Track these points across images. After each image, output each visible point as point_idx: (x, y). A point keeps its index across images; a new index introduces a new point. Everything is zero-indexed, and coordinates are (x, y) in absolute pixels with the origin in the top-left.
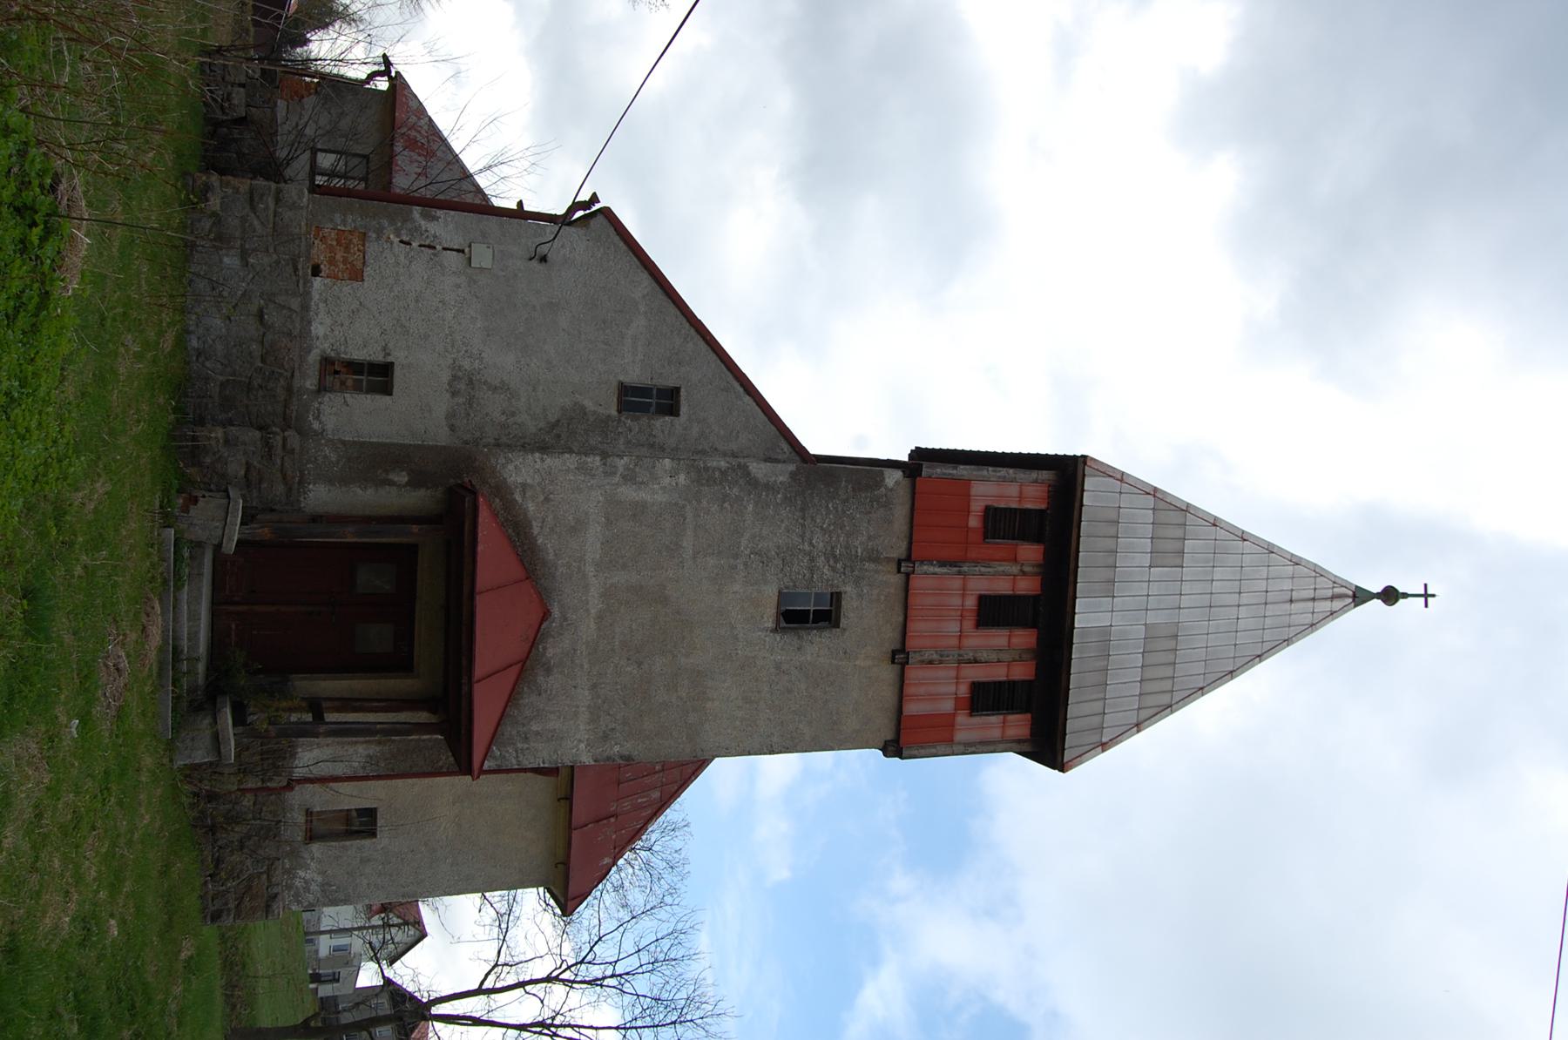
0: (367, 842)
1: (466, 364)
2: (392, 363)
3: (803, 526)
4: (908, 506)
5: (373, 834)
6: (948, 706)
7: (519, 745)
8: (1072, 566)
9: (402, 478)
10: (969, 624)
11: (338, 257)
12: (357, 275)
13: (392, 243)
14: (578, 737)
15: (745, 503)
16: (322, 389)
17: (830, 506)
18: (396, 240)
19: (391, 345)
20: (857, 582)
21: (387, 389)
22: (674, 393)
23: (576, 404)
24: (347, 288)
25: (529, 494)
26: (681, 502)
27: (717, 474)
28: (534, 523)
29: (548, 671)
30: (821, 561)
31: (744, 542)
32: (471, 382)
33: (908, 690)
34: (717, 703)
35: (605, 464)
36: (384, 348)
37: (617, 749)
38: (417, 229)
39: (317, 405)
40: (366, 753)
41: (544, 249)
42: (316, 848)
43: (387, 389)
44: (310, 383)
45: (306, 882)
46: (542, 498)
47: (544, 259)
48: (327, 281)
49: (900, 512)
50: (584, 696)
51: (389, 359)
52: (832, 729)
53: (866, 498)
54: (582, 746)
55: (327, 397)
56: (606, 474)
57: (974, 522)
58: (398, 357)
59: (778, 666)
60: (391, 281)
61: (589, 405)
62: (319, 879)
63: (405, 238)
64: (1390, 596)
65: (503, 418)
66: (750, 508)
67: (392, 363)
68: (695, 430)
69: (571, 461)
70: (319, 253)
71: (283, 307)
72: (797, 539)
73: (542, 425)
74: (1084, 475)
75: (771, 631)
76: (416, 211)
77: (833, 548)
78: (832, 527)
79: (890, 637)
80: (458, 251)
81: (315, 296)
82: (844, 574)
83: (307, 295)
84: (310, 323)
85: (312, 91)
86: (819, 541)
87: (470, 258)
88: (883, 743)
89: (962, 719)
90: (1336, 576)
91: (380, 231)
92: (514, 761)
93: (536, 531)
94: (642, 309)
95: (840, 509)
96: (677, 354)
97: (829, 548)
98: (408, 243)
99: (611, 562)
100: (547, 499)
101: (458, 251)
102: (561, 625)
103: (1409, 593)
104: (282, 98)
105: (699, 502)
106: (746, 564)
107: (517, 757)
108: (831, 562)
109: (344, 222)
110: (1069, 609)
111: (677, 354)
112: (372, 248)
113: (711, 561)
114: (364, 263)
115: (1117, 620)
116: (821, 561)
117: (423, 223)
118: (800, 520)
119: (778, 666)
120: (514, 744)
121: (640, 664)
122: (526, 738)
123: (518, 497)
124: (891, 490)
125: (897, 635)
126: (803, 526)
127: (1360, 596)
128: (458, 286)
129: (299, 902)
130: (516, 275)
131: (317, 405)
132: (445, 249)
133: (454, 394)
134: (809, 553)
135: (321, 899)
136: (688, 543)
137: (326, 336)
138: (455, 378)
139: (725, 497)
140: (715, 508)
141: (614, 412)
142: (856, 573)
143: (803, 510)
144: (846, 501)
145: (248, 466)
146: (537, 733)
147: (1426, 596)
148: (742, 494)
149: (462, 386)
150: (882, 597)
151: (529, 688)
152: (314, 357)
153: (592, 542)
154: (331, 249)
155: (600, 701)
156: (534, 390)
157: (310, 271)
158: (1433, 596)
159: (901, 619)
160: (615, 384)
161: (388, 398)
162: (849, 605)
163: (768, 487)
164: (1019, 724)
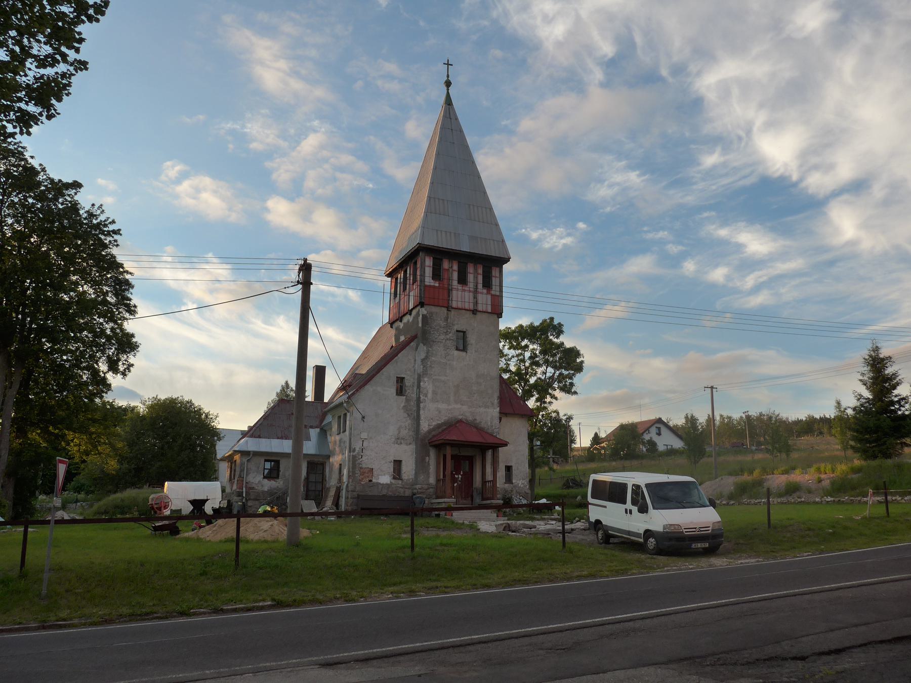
1: (393, 440)
3: (438, 342)
6: (489, 297)
8: (450, 250)
21: (400, 461)
24: (375, 473)
25: (430, 424)
26: (432, 380)
29: (475, 419)
30: (448, 337)
31: (442, 361)
32: (398, 439)
33: (484, 310)
34: (485, 371)
37: (496, 401)
42: (514, 481)
44: (400, 482)
46: (432, 421)
50: (482, 410)
58: (392, 459)
61: (403, 404)
62: (521, 480)
64: (448, 84)
66: (433, 358)
68: (408, 372)
79: (469, 314)
86: (442, 337)
91: (360, 464)
98: (362, 456)
100: (432, 419)
105: (432, 374)
106: (449, 360)
109: (358, 474)
110: (463, 253)
112: (364, 466)
116: (448, 337)
119: (476, 351)
121: (474, 393)
125: (468, 312)
126: (438, 342)
127: (448, 101)
133: (401, 443)
134: (446, 340)
136: (443, 378)
139: (430, 366)
149: (399, 441)
152: (393, 481)
153: (443, 406)
158: (452, 65)
164: (495, 272)
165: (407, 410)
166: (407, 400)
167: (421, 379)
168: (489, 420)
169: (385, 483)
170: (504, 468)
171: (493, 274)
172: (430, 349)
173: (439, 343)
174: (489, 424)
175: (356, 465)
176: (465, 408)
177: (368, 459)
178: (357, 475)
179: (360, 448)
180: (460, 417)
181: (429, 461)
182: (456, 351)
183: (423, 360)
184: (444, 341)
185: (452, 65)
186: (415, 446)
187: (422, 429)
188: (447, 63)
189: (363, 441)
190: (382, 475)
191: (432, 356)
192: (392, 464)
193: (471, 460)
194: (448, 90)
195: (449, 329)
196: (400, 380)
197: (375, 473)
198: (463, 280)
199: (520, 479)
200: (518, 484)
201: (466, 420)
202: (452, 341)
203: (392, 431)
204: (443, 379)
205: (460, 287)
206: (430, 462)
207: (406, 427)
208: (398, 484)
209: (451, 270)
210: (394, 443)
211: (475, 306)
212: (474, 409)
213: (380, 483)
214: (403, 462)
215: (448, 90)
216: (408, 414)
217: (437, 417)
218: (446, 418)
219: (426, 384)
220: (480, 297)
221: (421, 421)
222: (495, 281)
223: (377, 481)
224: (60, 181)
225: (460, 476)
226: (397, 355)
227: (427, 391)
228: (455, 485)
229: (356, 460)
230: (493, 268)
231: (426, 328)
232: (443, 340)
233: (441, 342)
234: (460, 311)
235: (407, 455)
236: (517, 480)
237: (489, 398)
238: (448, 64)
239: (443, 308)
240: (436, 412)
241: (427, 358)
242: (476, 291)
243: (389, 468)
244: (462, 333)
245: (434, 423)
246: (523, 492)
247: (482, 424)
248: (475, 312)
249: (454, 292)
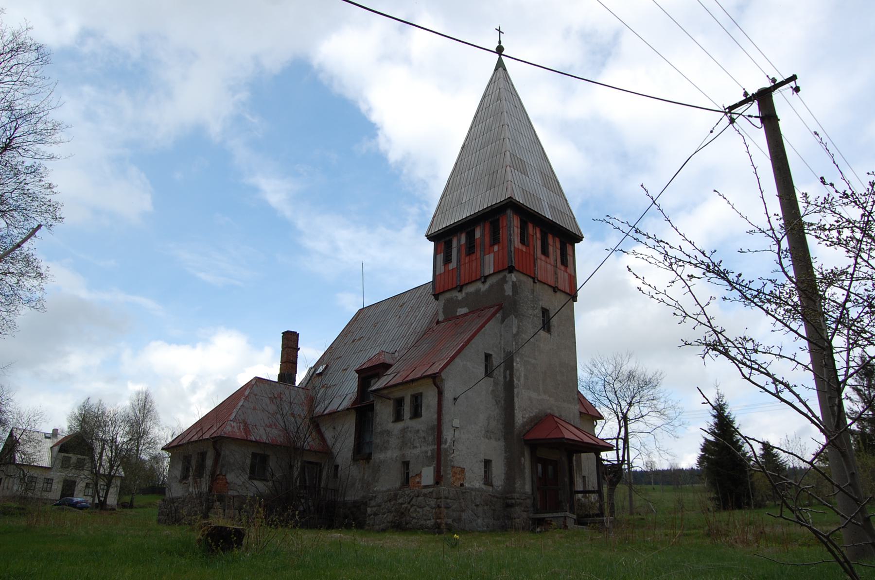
5: (464, 468)
6: (566, 275)
9: (523, 459)
12: (463, 470)
16: (492, 486)
18: (453, 455)
32: (488, 431)
51: (483, 461)
55: (494, 483)
61: (491, 388)
67: (485, 459)
70: (458, 484)
76: (443, 446)
79: (550, 291)
81: (469, 486)
83: (469, 488)
84: (476, 488)
85: (224, 478)
86: (530, 312)
93: (532, 415)
98: (453, 450)
103: (498, 40)
104: (228, 492)
109: (450, 474)
112: (456, 464)
114: (459, 467)
117: (448, 442)
123: (525, 420)
136: (533, 361)
137: (479, 483)
141: (492, 379)
145: (524, 511)
152: (484, 487)
153: (534, 395)
159: (546, 286)
162: (546, 306)
163: (519, 327)
164: (569, 248)
166: (496, 384)
167: (514, 359)
172: (521, 324)
177: (459, 455)
178: (448, 476)
179: (451, 440)
181: (524, 463)
184: (532, 317)
185: (496, 29)
186: (504, 443)
187: (517, 422)
189: (454, 430)
192: (483, 463)
195: (536, 304)
196: (488, 357)
197: (467, 475)
198: (545, 252)
206: (525, 465)
207: (495, 417)
214: (493, 462)
216: (496, 401)
219: (519, 365)
221: (515, 411)
222: (569, 258)
226: (484, 326)
235: (495, 450)
238: (500, 32)
239: (529, 278)
243: (480, 469)
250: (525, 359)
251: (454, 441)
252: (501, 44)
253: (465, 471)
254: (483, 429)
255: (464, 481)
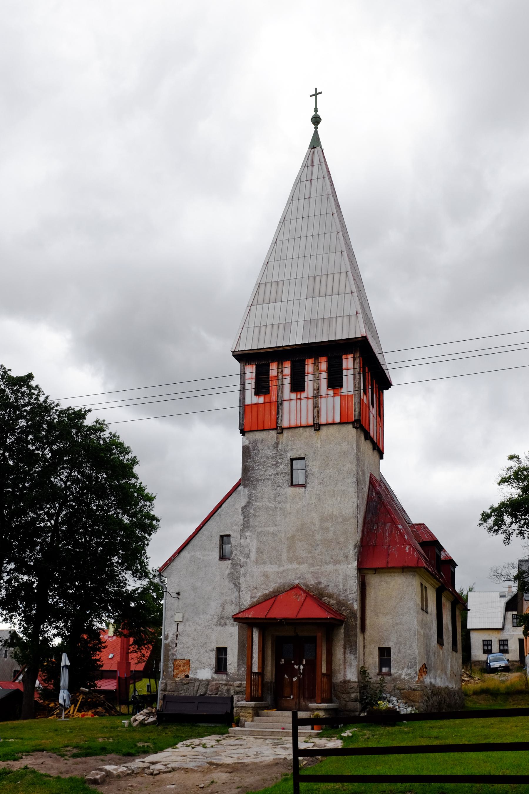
0: (392, 651)
1: (215, 620)
2: (216, 648)
3: (264, 480)
4: (256, 433)
6: (338, 399)
7: (348, 592)
8: (276, 349)
10: (304, 395)
11: (182, 669)
13: (177, 650)
14: (346, 568)
15: (256, 506)
17: (256, 468)
19: (210, 649)
20: (286, 451)
21: (225, 649)
22: (222, 537)
23: (228, 577)
24: (192, 665)
25: (254, 595)
26: (256, 533)
27: (246, 519)
28: (265, 593)
29: (320, 583)
30: (278, 470)
31: (270, 505)
32: (221, 618)
33: (330, 421)
34: (334, 510)
35: (243, 566)
36: (211, 651)
37: (351, 552)
38: (171, 641)
39: (231, 675)
40: (349, 654)
41: (175, 595)
43: (225, 649)
44: (224, 677)
45: (407, 675)
46: (256, 590)
47: (178, 594)
48: (190, 672)
49: (258, 436)
50: (330, 568)
51: (215, 649)
52: (347, 454)
53: (253, 452)
54: (350, 566)
56: (247, 565)
57: (261, 400)
58: (214, 646)
59: (320, 484)
60: (189, 650)
61: (228, 571)
62: (405, 670)
63: (175, 645)
64: (316, 120)
65: (233, 605)
66: (258, 504)
67: (216, 648)
68: (235, 527)
69: (242, 580)
70: (182, 676)
71: (198, 688)
72: (270, 482)
73: (235, 590)
74: (239, 351)
75: (305, 488)
77: (273, 465)
78: (265, 467)
79: (310, 432)
80: (178, 626)
82: (283, 458)
86: (270, 471)
87: (180, 621)
88: (354, 429)
89: (344, 391)
90: (302, 166)
91: (174, 655)
92: (354, 595)
93: (267, 592)
94: (193, 553)
95: (258, 464)
96: (208, 537)
97: (273, 467)
98: (176, 644)
99: (279, 561)
100: (256, 588)
101: (178, 626)
102: (302, 579)
105: (256, 526)
106: (279, 503)
107: (353, 593)
108: (278, 465)
109: (171, 667)
110: (294, 347)
111: (208, 537)
112: (179, 657)
113: (278, 518)
114: (184, 659)
115: (301, 319)
116: (278, 470)
118: (262, 481)
119: (320, 484)
120: (348, 595)
121: (318, 545)
122: (345, 590)
123: (255, 600)
124: (250, 441)
125: (308, 429)
126: (264, 480)
127: (315, 143)
128: (189, 625)
129: (414, 677)
130: (185, 604)
131: (231, 675)
132: (177, 631)
133: (226, 624)
134: (275, 475)
135: (414, 669)
136: (271, 529)
138: (220, 624)
139: (254, 515)
140: (258, 519)
141: (230, 561)
142: (283, 453)
143: (258, 481)
144: (254, 461)
146: (344, 586)
147: (316, 94)
148: (253, 508)
149: (223, 621)
150: (293, 439)
151: (326, 590)
152: (215, 676)
153: (270, 569)
154: (180, 672)
155: (332, 560)
156: (223, 594)
157: (187, 679)
158: (316, 89)
159: (301, 429)
160: (220, 562)
161: (228, 649)
165: (233, 579)
168: (341, 580)
169: (204, 679)
170: (376, 652)
171: (344, 366)
173: (266, 481)
174: (341, 587)
175: (169, 657)
176: (304, 568)
180: (297, 582)
182: (290, 488)
183: (244, 508)
185: (316, 89)
188: (318, 92)
189: (178, 624)
190: (201, 668)
191: (256, 501)
192: (214, 652)
193: (313, 640)
194: (316, 128)
199: (403, 668)
200: (401, 674)
201: (307, 586)
202: (284, 475)
203: (214, 608)
204: (272, 530)
205: (293, 396)
207: (232, 601)
208: (222, 680)
209: (280, 376)
210: (217, 625)
211: (316, 418)
212: (318, 567)
213: (198, 679)
215: (316, 128)
217: (262, 584)
218: (277, 585)
219: (248, 541)
220: (323, 402)
223: (195, 677)
224: (17, 377)
225: (302, 667)
227: (249, 550)
228: (295, 679)
229: (169, 650)
230: (344, 357)
231: (248, 464)
232: (271, 475)
233: (268, 479)
234: (297, 430)
236: (398, 670)
237: (341, 549)
239: (271, 431)
240: (262, 578)
241: (249, 504)
242: (317, 396)
244: (294, 462)
245: (259, 594)
246: (407, 687)
247: (330, 588)
248: (317, 427)
249: (286, 404)
250: (260, 530)
251: (177, 634)
252: (318, 113)
253: (191, 662)
254: (215, 616)
255: (189, 672)
